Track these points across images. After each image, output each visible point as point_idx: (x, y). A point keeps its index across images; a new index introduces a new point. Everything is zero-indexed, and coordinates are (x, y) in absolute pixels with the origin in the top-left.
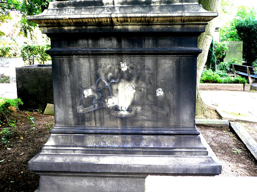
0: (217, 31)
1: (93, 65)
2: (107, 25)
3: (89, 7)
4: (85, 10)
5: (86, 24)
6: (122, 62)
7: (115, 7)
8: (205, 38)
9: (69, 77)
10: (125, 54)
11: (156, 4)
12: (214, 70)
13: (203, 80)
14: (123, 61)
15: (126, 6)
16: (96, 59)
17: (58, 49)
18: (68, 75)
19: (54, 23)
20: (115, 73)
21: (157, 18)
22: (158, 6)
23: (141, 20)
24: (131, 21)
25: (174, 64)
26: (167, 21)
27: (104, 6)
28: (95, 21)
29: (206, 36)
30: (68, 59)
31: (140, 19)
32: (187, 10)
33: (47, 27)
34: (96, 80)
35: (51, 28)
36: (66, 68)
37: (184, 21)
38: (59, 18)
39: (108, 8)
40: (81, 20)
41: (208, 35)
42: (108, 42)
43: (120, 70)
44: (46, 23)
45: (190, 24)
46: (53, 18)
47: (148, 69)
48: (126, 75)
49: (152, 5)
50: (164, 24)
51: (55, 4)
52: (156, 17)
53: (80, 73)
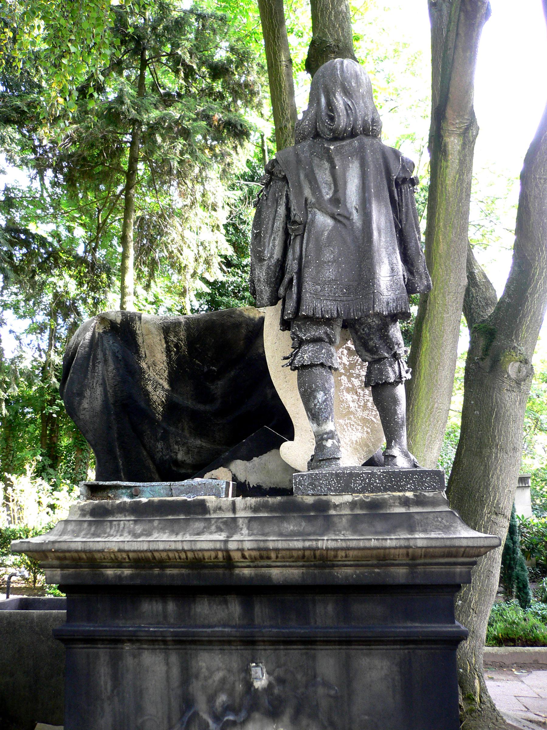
0: (524, 485)
1: (175, 671)
2: (215, 566)
3: (170, 517)
4: (160, 526)
5: (162, 564)
6: (254, 664)
7: (238, 519)
8: (488, 522)
9: (110, 705)
10: (264, 641)
11: (341, 510)
12: (524, 603)
13: (495, 638)
14: (258, 661)
15: (266, 515)
16: (186, 653)
17: (87, 627)
18: (109, 698)
19: (80, 559)
20: (237, 694)
21: (344, 552)
22: (345, 517)
23: (304, 556)
24: (277, 557)
25: (395, 669)
26: (372, 557)
27: (210, 514)
28: (187, 557)
29: (490, 517)
30: (110, 652)
31: (300, 552)
32: (421, 526)
33: (62, 567)
34: (183, 713)
35: (71, 571)
36: (103, 678)
37: (414, 558)
38: (94, 549)
39: (220, 520)
40: (149, 555)
41: (496, 514)
42: (219, 607)
43: (249, 685)
44: (58, 558)
45: (431, 564)
46: (80, 549)
47: (326, 684)
48: (265, 701)
49: (332, 512)
50: (362, 566)
51: (86, 507)
52: (342, 549)
53: (139, 693)
